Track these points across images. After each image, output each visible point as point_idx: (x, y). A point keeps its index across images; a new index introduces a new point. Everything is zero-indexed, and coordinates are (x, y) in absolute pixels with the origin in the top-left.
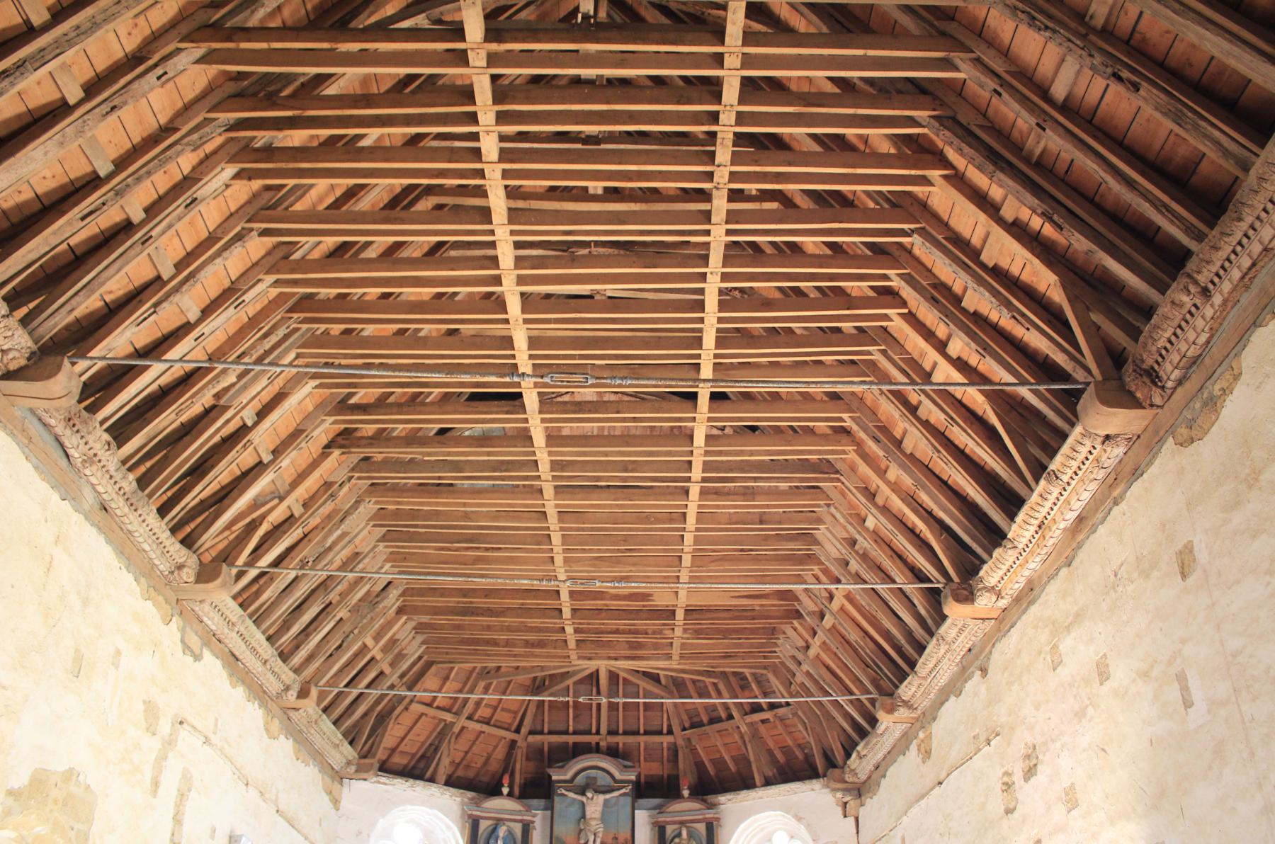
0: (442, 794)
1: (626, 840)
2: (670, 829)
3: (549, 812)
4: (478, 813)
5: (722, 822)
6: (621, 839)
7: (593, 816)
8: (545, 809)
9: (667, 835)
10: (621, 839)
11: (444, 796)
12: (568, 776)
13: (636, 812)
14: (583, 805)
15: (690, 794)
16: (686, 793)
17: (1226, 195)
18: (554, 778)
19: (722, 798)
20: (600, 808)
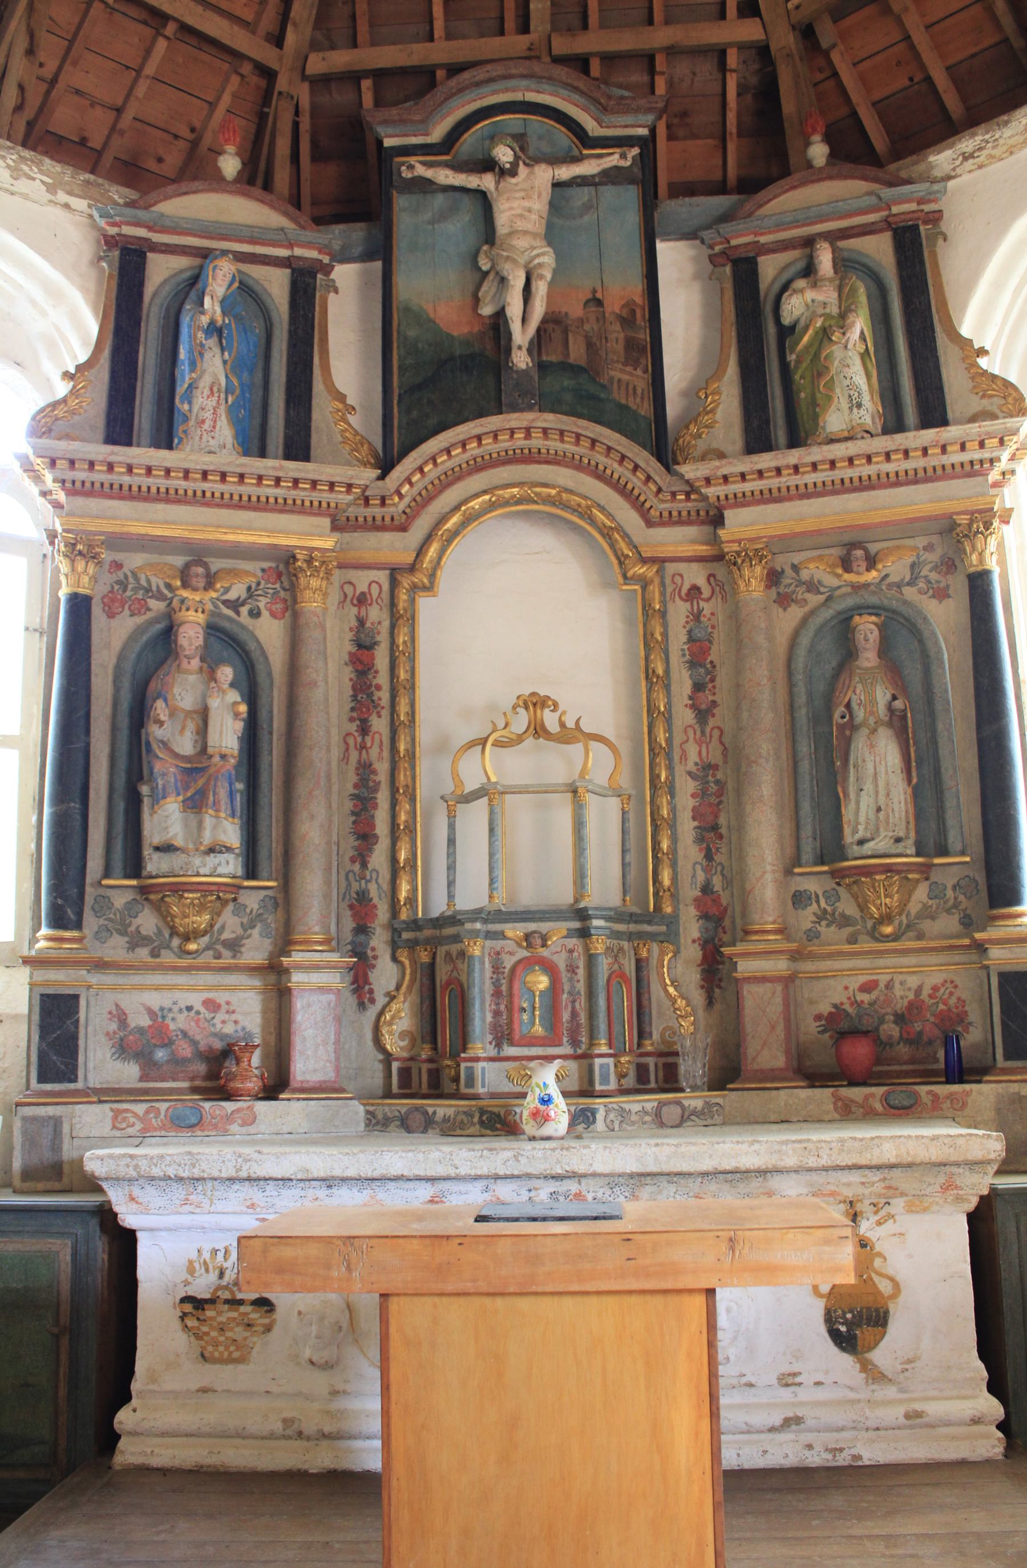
0: (314, 684)
1: (630, 306)
2: (769, 268)
3: (379, 264)
4: (142, 232)
5: (946, 215)
6: (614, 305)
7: (520, 225)
8: (367, 257)
9: (763, 286)
10: (614, 305)
11: (23, 185)
12: (437, 134)
13: (660, 246)
14: (483, 200)
15: (834, 155)
16: (819, 152)
17: (362, 1351)
18: (388, 142)
19: (941, 159)
20: (539, 205)
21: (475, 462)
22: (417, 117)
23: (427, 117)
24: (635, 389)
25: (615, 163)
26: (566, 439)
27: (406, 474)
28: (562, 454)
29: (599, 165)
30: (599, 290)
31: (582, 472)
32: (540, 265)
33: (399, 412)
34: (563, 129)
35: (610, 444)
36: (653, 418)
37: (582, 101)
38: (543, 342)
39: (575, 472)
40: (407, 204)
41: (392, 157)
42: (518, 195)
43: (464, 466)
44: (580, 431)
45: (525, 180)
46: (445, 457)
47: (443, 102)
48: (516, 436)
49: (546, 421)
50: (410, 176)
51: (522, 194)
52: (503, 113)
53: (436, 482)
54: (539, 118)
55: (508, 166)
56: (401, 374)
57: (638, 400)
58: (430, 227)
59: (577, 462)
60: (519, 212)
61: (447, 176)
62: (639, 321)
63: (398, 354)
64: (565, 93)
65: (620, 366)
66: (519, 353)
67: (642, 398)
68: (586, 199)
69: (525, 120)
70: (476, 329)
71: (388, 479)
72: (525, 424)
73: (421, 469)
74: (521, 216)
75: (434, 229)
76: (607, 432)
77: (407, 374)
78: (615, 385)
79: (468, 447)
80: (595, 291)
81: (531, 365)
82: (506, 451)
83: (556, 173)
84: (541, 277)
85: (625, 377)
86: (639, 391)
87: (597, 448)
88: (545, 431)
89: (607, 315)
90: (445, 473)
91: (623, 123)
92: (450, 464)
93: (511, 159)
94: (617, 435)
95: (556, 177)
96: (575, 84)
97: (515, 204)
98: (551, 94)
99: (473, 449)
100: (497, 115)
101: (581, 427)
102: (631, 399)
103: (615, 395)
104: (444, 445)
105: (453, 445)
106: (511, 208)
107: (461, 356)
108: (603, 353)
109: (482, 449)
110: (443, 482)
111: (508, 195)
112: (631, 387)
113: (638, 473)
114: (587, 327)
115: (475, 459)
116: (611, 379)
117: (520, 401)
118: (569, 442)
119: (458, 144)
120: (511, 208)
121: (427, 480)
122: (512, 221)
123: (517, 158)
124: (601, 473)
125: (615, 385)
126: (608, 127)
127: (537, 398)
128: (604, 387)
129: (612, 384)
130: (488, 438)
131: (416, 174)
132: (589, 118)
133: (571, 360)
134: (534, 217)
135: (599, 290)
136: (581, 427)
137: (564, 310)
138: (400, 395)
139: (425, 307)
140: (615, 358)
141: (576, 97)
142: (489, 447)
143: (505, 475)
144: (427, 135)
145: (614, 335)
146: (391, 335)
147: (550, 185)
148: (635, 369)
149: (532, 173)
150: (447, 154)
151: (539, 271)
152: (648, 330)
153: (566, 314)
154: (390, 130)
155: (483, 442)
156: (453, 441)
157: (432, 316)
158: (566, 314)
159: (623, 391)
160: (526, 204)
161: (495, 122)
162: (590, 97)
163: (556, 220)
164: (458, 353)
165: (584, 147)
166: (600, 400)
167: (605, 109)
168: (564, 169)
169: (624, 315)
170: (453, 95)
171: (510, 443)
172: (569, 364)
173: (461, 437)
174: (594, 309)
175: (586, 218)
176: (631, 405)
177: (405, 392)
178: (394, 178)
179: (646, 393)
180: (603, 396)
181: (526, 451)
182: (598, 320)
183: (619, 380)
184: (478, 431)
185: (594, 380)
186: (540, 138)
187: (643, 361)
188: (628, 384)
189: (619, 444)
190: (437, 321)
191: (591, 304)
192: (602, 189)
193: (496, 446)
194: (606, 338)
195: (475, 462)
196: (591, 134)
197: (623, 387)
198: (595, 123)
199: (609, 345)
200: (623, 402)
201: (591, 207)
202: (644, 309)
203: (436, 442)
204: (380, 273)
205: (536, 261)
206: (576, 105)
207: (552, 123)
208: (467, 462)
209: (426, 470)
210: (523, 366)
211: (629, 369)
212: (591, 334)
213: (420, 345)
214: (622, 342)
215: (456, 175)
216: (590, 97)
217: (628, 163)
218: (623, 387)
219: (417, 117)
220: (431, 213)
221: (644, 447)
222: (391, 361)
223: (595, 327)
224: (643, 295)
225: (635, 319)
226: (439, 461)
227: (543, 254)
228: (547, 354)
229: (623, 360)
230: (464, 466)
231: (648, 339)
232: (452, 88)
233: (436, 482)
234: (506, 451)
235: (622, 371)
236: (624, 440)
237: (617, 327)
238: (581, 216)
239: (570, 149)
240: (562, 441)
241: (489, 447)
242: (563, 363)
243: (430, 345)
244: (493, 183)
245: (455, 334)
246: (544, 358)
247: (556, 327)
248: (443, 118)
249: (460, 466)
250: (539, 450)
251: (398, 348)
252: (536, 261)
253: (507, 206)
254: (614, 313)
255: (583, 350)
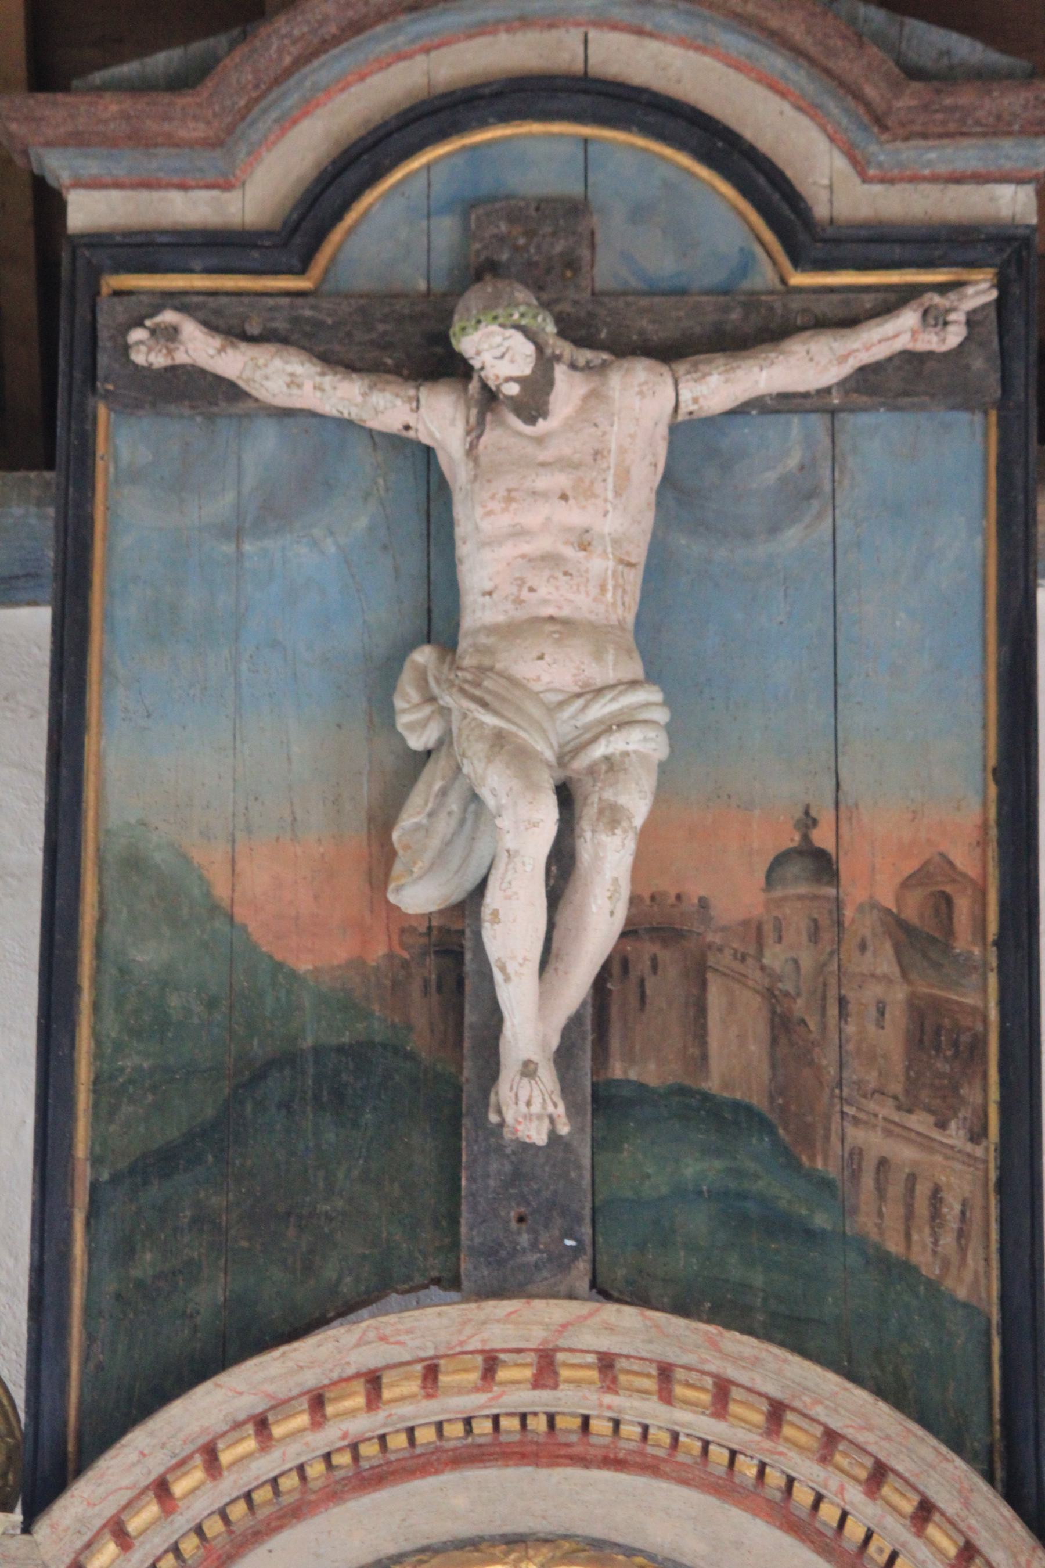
21: (356, 1457)
22: (197, 130)
23: (230, 130)
24: (936, 1196)
25: (903, 343)
26: (679, 1391)
27: (109, 1510)
28: (666, 1439)
29: (843, 359)
30: (826, 817)
31: (737, 1504)
32: (611, 764)
33: (91, 1254)
34: (726, 188)
35: (835, 1424)
36: (995, 1317)
37: (799, 77)
38: (614, 1010)
39: (710, 1501)
40: (144, 455)
41: (95, 274)
42: (544, 481)
43: (316, 1470)
44: (731, 1372)
45: (569, 425)
46: (250, 1444)
47: (288, 73)
48: (502, 1374)
49: (611, 1329)
50: (159, 360)
51: (561, 480)
52: (505, 118)
53: (214, 1527)
54: (641, 142)
55: (513, 389)
56: (101, 1114)
57: (948, 1241)
58: (228, 548)
59: (721, 1470)
60: (544, 544)
61: (294, 382)
62: (964, 942)
63: (97, 1037)
64: (736, 43)
65: (886, 1110)
66: (525, 1088)
67: (961, 1234)
68: (793, 462)
69: (586, 141)
70: (378, 952)
71: (43, 1528)
72: (536, 1337)
73: (162, 1488)
74: (550, 560)
75: (240, 555)
76: (829, 1381)
77: (127, 1109)
78: (868, 1181)
79: (330, 1409)
80: (808, 821)
81: (564, 1129)
82: (468, 1422)
83: (686, 395)
84: (613, 816)
85: (905, 1154)
86: (952, 1209)
87: (787, 1431)
88: (606, 1363)
89: (849, 913)
90: (248, 1496)
91: (942, 169)
92: (266, 1466)
93: (524, 367)
94: (861, 1396)
95: (685, 407)
96: (774, 23)
97: (533, 516)
98: (684, 42)
99: (352, 1413)
100: (483, 124)
101: (736, 1360)
102: (922, 1236)
103: (865, 1222)
104: (250, 1404)
105: (282, 1405)
106: (519, 533)
107: (318, 1051)
108: (828, 1060)
109: (381, 1415)
110: (238, 1529)
111: (510, 481)
112: (923, 1190)
113: (932, 1530)
114: (775, 957)
115: (354, 1448)
116: (857, 1154)
117: (524, 1239)
118: (687, 1403)
119: (336, 235)
120: (519, 533)
121: (182, 1521)
122: (521, 582)
123: (545, 362)
124: (803, 1512)
125: (868, 1181)
126: (885, 180)
127: (586, 1230)
128: (826, 1184)
129: (856, 1176)
130: (407, 1378)
131: (181, 358)
132: (822, 144)
133: (713, 1085)
134: (600, 565)
135: (826, 817)
136: (736, 1360)
137: (695, 890)
138: (95, 1187)
139: (198, 857)
140: (872, 1079)
141: (777, 62)
142: (406, 1409)
143: (460, 1502)
144: (226, 186)
145: (874, 991)
146: (74, 963)
147: (663, 430)
148: (942, 1125)
149: (594, 395)
150: (302, 270)
151: (608, 795)
152: (993, 980)
153: (704, 904)
154: (92, 167)
155: (387, 1394)
156: (281, 1390)
157: (221, 891)
158: (704, 904)
159: (893, 1211)
160: (573, 516)
161: (475, 147)
162: (827, 71)
163: (681, 540)
164: (309, 1042)
165: (798, 261)
166: (811, 1235)
167: (879, 121)
168: (715, 379)
169: (911, 914)
170: (326, 45)
171: (482, 1398)
172: (706, 1097)
173: (311, 1379)
174: (803, 889)
175: (792, 536)
176: (922, 1259)
177: (116, 1179)
178: (103, 360)
179: (976, 1215)
180: (821, 1220)
181: (538, 1424)
182: (815, 933)
183: (883, 1163)
184: (369, 1358)
185: (793, 1164)
186: (639, 213)
187: (971, 1093)
188: (912, 1179)
189: (869, 1428)
190: (241, 914)
191: (794, 869)
192: (853, 423)
193: (432, 1405)
194: (842, 1002)
195: (356, 1457)
196: (821, 211)
197: (896, 1189)
198: (841, 163)
199: (851, 1029)
200: (894, 1246)
201: (811, 494)
202: (984, 892)
203: (219, 1395)
204: (42, 653)
205: (599, 750)
206: (773, 87)
207: (684, 160)
208: (327, 1457)
209: (179, 1488)
210: (538, 1135)
211: (920, 1122)
212: (788, 986)
213: (174, 1001)
214: (897, 1016)
215: (328, 380)
216: (827, 71)
217: (954, 336)
218: (896, 1189)
219: (197, 130)
220: (230, 497)
221: (957, 1447)
222: (70, 1064)
223: (807, 962)
224: (983, 844)
225: (950, 932)
226: (226, 1457)
227: (622, 722)
228: (630, 1058)
229: (896, 1087)
230: (316, 1470)
231: (993, 1014)
232: (325, 20)
233: (214, 1527)
234: (468, 1422)
235: (891, 1129)
236: (883, 1413)
237: (885, 962)
238: (774, 530)
239: (746, 265)
240: (666, 1396)
241: (406, 1409)
242: (682, 1091)
243: (212, 1004)
244: (460, 428)
245: (304, 966)
246: (617, 1070)
247: (665, 955)
248: (288, 122)
249: (301, 1469)
250: (586, 1420)
251: (96, 1007)
252: (599, 750)
253: (504, 521)
254: (874, 905)
255: (757, 1049)
